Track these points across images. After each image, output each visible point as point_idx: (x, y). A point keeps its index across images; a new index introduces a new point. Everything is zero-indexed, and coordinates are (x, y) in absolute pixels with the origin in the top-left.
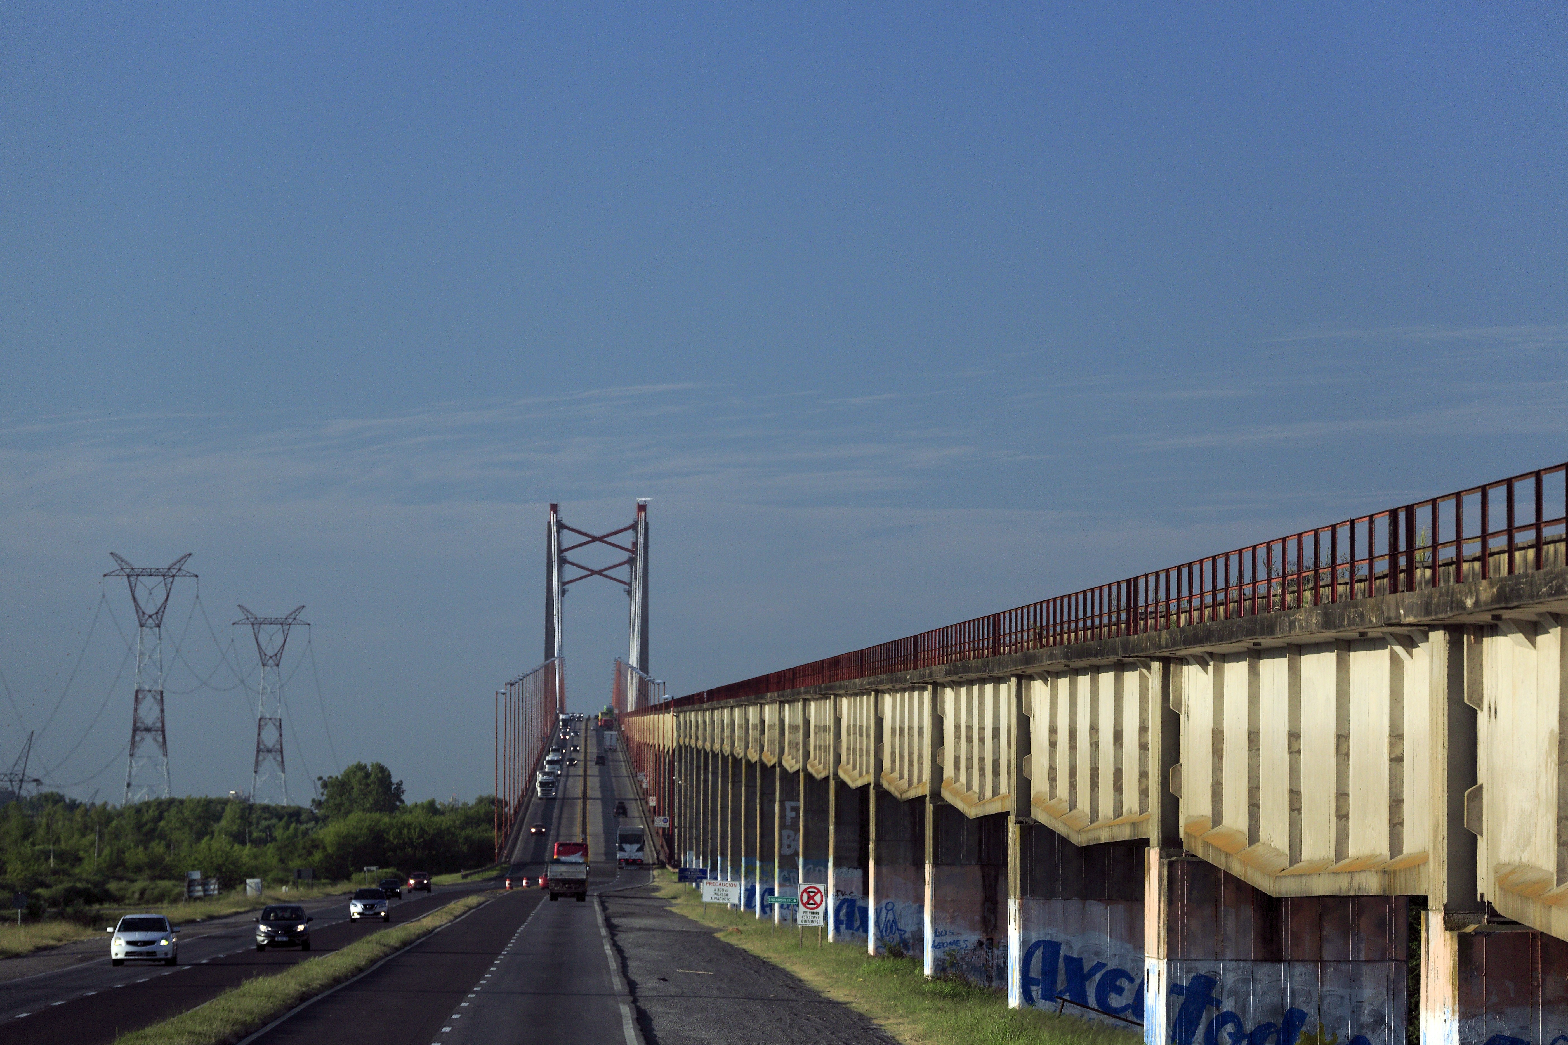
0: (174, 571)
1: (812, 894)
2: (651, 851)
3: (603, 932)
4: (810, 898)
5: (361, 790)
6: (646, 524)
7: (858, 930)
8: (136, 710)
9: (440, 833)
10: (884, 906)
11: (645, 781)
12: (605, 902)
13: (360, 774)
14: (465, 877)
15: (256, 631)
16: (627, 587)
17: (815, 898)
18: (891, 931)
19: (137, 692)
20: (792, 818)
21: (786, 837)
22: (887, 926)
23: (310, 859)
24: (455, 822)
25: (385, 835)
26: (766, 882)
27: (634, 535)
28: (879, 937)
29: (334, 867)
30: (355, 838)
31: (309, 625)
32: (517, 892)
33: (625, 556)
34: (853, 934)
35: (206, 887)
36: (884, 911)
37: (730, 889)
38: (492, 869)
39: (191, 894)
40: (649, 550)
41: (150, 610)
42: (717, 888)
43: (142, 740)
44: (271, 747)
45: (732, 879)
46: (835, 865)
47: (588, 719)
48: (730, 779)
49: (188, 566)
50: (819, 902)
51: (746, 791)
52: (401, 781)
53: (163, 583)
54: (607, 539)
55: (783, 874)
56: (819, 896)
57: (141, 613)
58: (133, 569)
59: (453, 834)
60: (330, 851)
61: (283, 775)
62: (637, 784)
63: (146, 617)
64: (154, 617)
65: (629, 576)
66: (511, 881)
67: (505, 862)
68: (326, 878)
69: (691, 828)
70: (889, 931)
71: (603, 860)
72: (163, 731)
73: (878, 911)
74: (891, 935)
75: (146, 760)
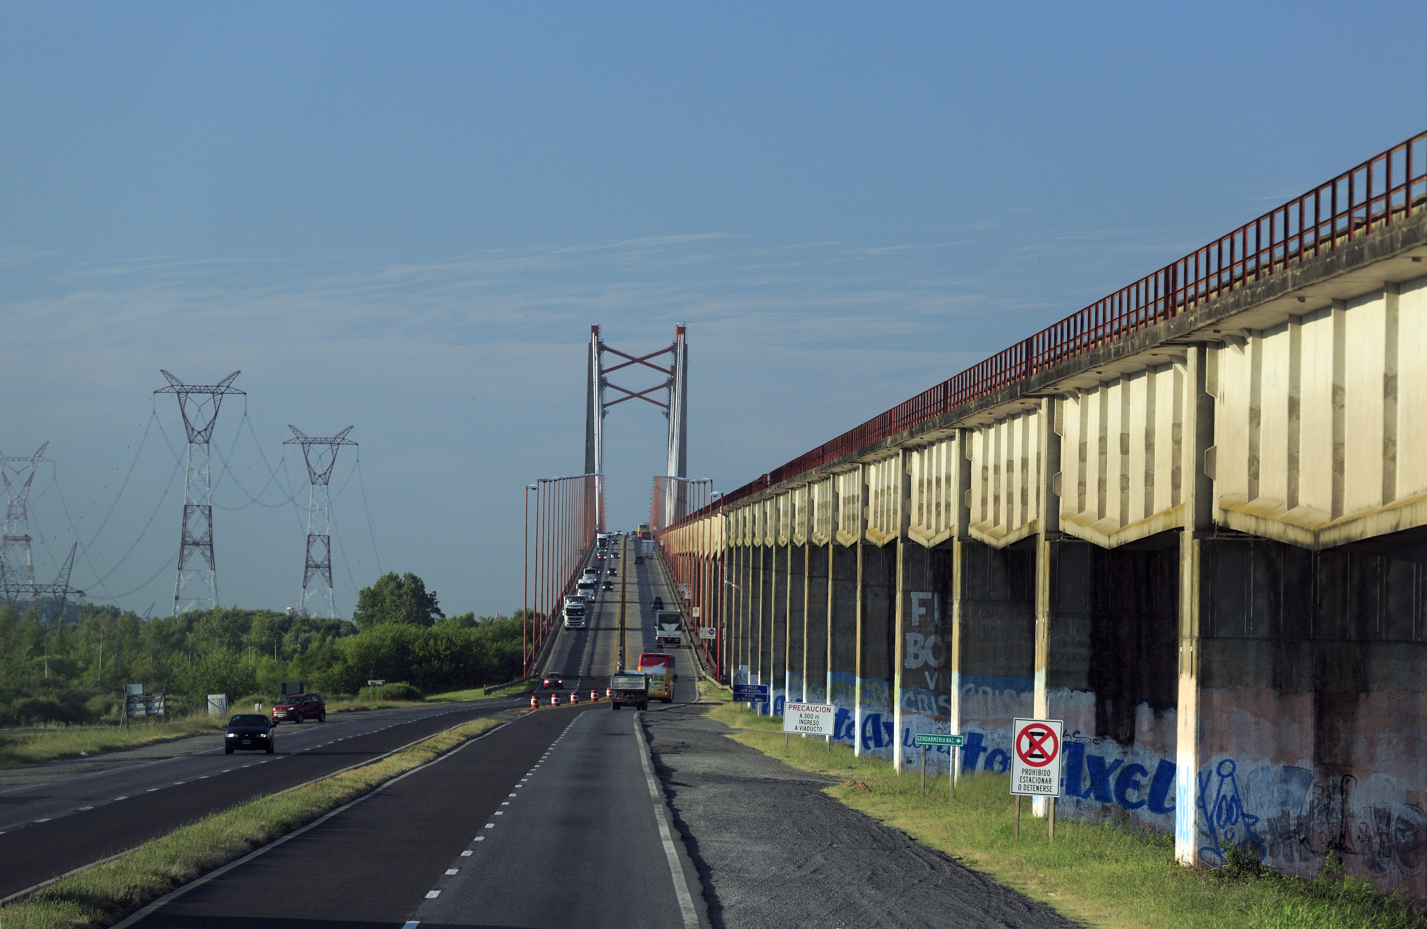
0: (223, 389)
1: (1037, 738)
2: (696, 665)
3: (653, 787)
4: (1033, 745)
5: (393, 601)
6: (685, 346)
7: (1086, 795)
8: (184, 525)
9: (468, 645)
10: (1214, 768)
11: (686, 592)
12: (648, 726)
13: (392, 585)
14: (488, 692)
15: (306, 451)
16: (665, 409)
17: (1043, 745)
18: (1229, 818)
19: (186, 507)
20: (920, 616)
21: (912, 642)
22: (1220, 808)
23: (329, 671)
24: (487, 634)
25: (410, 647)
26: (869, 705)
27: (674, 357)
28: (1205, 828)
29: (355, 680)
30: (377, 649)
31: (245, 394)
32: (542, 713)
33: (665, 377)
34: (1078, 801)
35: (150, 705)
36: (1215, 778)
37: (821, 714)
38: (519, 684)
39: (130, 713)
40: (688, 371)
41: (200, 426)
42: (803, 713)
43: (190, 553)
44: (319, 563)
45: (809, 701)
46: (1051, 684)
47: (627, 536)
48: (807, 574)
49: (350, 437)
50: (1050, 752)
51: (834, 585)
52: (435, 592)
53: (212, 399)
54: (646, 361)
55: (907, 695)
56: (1050, 740)
57: (190, 430)
59: (483, 647)
60: (350, 663)
62: (677, 596)
63: (196, 433)
64: (202, 433)
65: (668, 399)
66: (537, 698)
67: (534, 677)
68: (346, 692)
69: (745, 638)
70: (1224, 817)
72: (211, 546)
73: (1204, 777)
74: (1229, 826)
75: (193, 574)
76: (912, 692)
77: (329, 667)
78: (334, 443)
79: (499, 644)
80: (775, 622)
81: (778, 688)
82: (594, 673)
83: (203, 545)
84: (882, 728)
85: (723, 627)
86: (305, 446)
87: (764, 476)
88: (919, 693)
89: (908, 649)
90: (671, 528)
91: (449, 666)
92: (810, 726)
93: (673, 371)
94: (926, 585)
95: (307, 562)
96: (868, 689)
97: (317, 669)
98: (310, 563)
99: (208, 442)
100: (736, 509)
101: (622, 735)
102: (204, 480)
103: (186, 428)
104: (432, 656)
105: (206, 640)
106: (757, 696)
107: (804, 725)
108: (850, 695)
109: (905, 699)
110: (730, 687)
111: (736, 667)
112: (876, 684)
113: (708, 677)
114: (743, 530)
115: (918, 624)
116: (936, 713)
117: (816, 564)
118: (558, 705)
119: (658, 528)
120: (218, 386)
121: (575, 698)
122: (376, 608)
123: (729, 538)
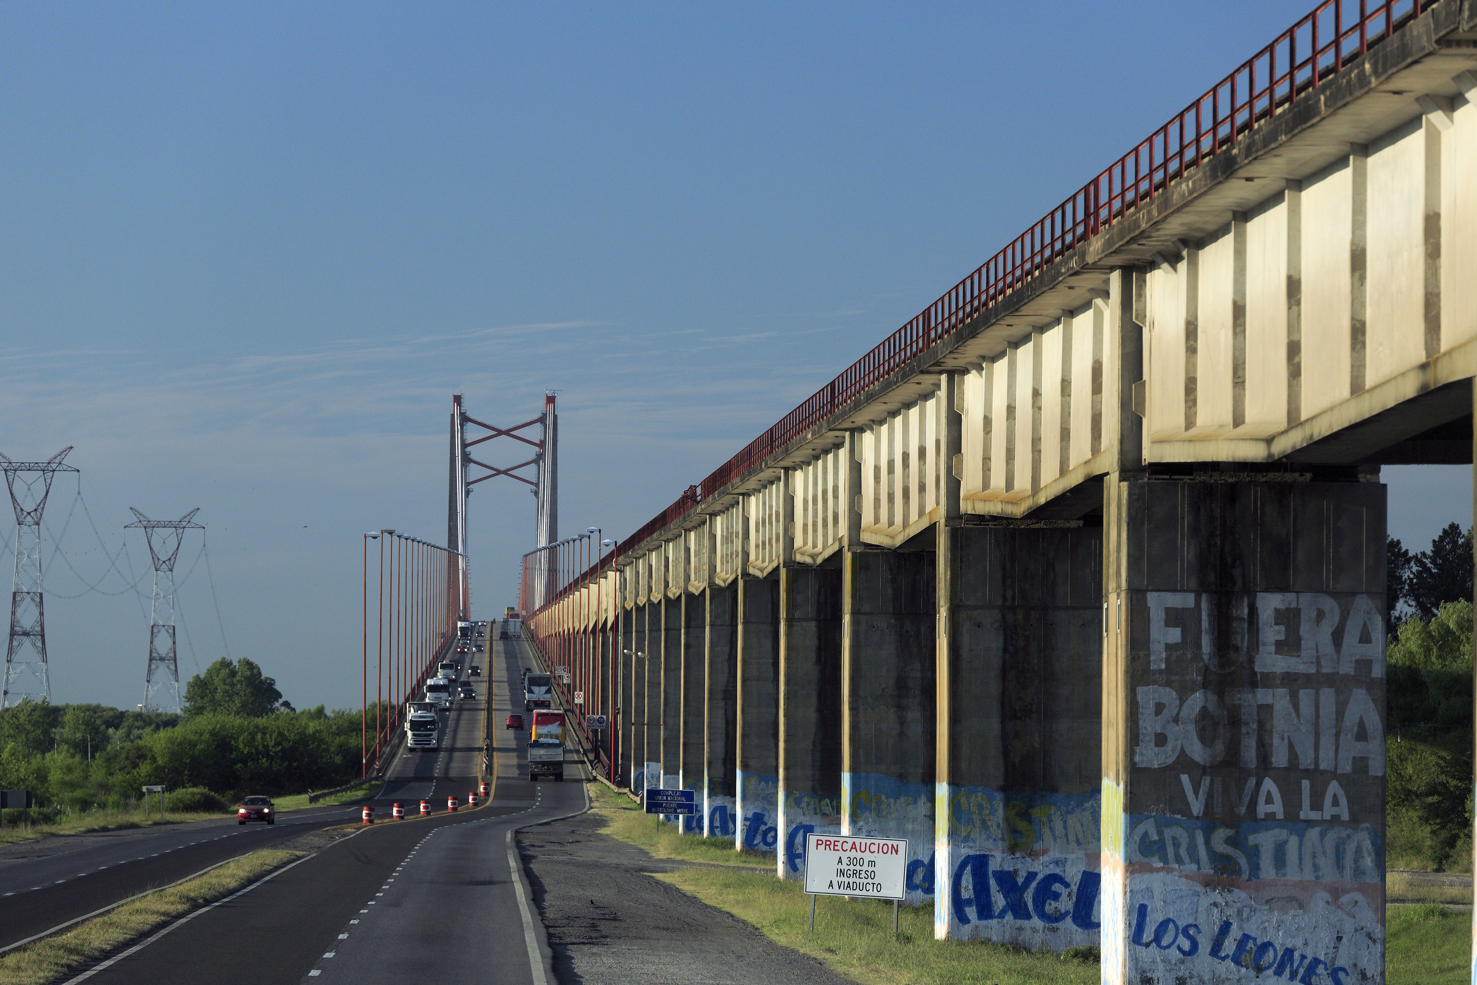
5: (227, 691)
6: (555, 417)
8: (13, 613)
13: (224, 672)
14: (313, 800)
19: (15, 594)
20: (1169, 647)
23: (135, 772)
24: (331, 728)
25: (233, 742)
26: (966, 839)
30: (193, 745)
31: (78, 471)
33: (532, 452)
37: (879, 858)
41: (29, 507)
42: (845, 856)
43: (20, 644)
44: (164, 655)
45: (857, 831)
49: (196, 519)
51: (855, 623)
53: (43, 478)
54: (513, 433)
55: (1141, 829)
57: (18, 510)
58: (10, 463)
59: (321, 741)
60: (160, 763)
61: (176, 685)
64: (32, 514)
67: (377, 778)
71: (516, 775)
72: (43, 636)
75: (23, 667)
76: (1151, 820)
77: (134, 768)
78: (178, 526)
79: (342, 738)
80: (710, 699)
81: (716, 795)
82: (453, 773)
83: (33, 635)
84: (992, 882)
85: (618, 713)
86: (148, 530)
87: (693, 488)
88: (1169, 824)
89: (1141, 723)
90: (542, 609)
91: (280, 765)
92: (858, 880)
93: (542, 444)
94: (1182, 576)
95: (151, 655)
96: (965, 806)
97: (120, 770)
98: (155, 655)
99: (38, 524)
100: (636, 558)
101: (491, 883)
102: (34, 565)
103: (15, 508)
104: (260, 753)
106: (680, 806)
107: (846, 880)
108: (884, 813)
109: (1137, 838)
110: (630, 790)
111: (640, 764)
112: (978, 797)
113: (599, 777)
114: (649, 582)
115: (1163, 666)
116: (1208, 870)
118: (402, 818)
119: (527, 612)
120: (49, 463)
123: (625, 599)
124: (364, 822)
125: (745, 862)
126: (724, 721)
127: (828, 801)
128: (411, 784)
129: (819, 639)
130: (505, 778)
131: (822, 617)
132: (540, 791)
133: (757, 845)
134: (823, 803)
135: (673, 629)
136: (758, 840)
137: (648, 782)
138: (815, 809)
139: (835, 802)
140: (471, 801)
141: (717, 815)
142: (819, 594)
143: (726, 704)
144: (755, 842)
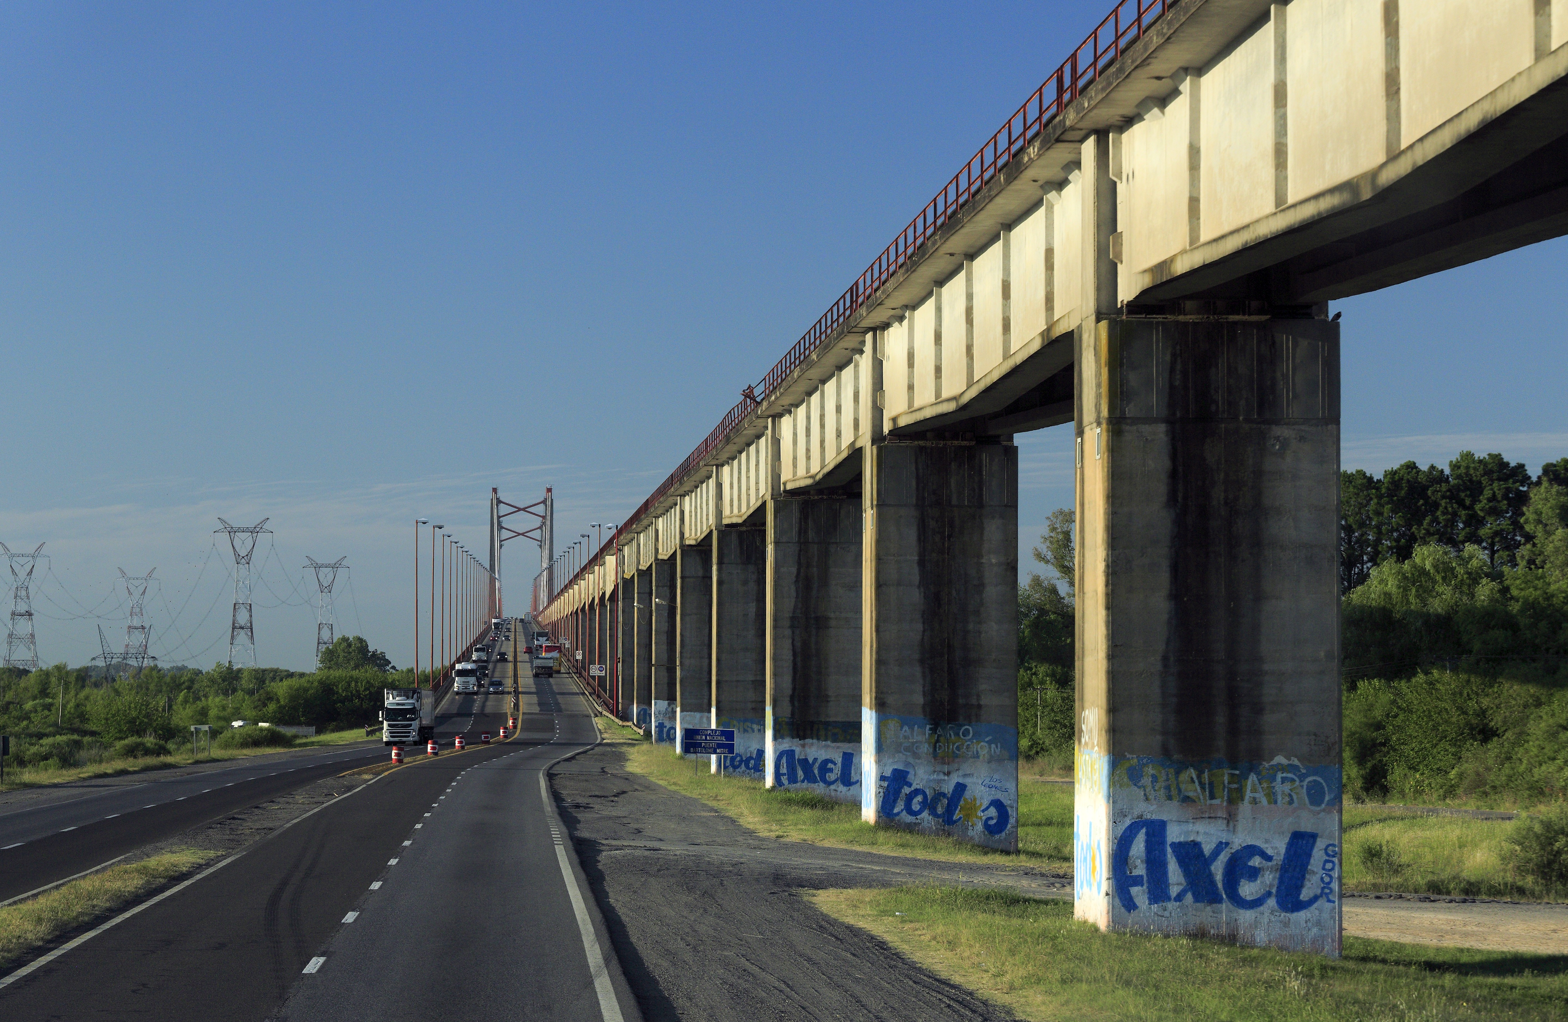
5: (344, 657)
6: (552, 500)
13: (344, 644)
14: (369, 733)
23: (264, 709)
30: (306, 690)
33: (538, 521)
49: (344, 563)
72: (252, 629)
75: (240, 647)
81: (782, 737)
82: (489, 710)
84: (1169, 850)
105: (208, 686)
106: (720, 746)
117: (1133, 379)
121: (460, 742)
122: (332, 663)
124: (393, 762)
125: (903, 846)
126: (791, 653)
127: (1193, 773)
128: (454, 719)
129: (1173, 457)
130: (529, 714)
131: (1178, 414)
132: (558, 724)
133: (898, 814)
134: (1184, 776)
135: (689, 577)
136: (899, 807)
137: (656, 717)
138: (1168, 788)
139: (1206, 775)
140: (501, 734)
141: (784, 760)
142: (1172, 371)
143: (793, 632)
144: (896, 811)
